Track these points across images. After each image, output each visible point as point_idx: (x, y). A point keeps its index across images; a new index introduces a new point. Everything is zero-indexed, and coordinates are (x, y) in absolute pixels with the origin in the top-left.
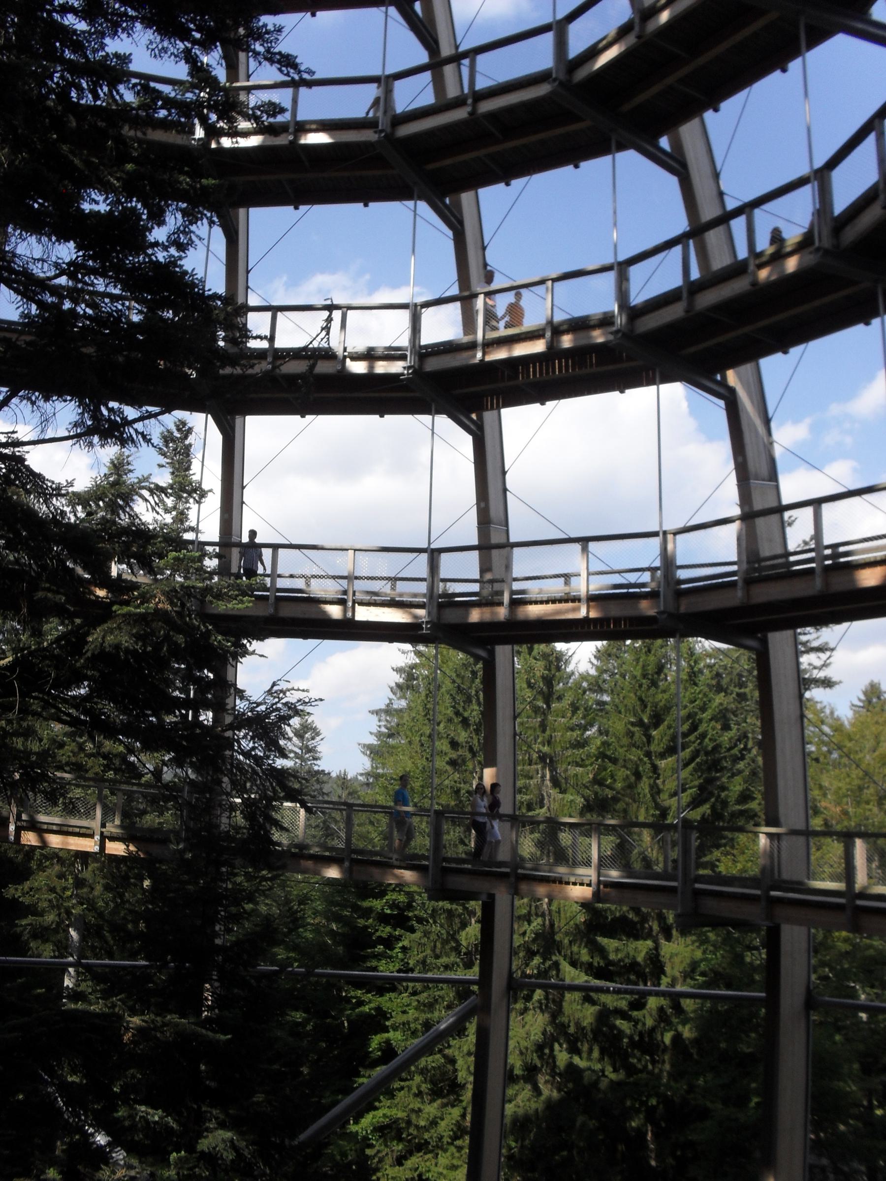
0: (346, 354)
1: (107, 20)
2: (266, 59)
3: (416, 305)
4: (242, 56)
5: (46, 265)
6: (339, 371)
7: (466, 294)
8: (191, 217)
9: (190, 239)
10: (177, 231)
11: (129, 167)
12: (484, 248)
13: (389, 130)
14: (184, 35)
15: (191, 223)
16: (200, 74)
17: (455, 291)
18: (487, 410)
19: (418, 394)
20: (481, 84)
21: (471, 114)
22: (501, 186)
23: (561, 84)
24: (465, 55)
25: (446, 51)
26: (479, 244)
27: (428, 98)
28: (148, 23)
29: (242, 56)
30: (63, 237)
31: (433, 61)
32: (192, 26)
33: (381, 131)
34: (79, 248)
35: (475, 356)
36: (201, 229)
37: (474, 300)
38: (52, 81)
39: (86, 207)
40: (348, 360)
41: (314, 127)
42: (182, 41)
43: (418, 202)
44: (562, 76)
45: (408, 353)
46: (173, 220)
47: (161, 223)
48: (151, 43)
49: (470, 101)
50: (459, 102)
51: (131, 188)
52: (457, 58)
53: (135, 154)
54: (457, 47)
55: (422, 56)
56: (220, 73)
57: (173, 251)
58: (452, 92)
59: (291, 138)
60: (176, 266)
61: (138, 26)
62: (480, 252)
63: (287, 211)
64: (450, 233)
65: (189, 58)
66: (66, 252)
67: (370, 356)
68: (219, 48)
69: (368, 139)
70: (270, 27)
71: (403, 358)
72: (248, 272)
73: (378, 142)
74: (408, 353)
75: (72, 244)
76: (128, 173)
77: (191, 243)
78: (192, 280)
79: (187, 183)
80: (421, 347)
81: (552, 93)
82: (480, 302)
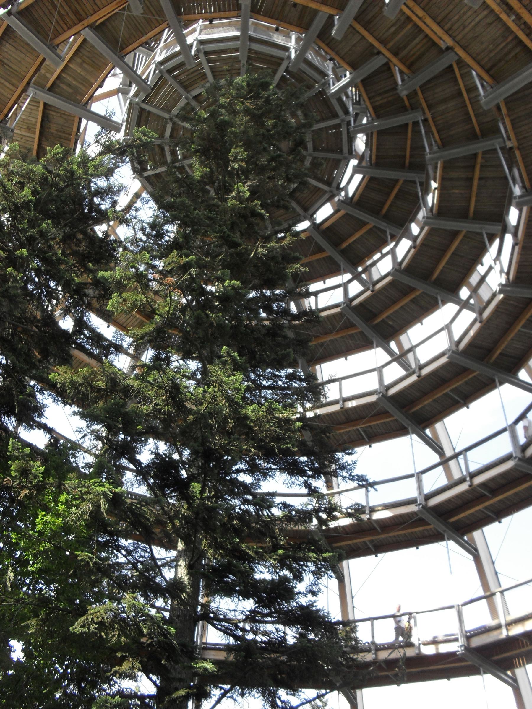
0: (420, 642)
1: (260, 473)
2: (350, 479)
3: (458, 606)
4: (334, 479)
5: (236, 613)
6: (417, 654)
7: (488, 594)
8: (318, 574)
9: (319, 588)
10: (312, 584)
11: (280, 552)
12: (493, 563)
13: (424, 503)
14: (302, 473)
15: (318, 578)
16: (313, 492)
17: (481, 593)
18: (517, 667)
19: (469, 663)
20: (473, 468)
21: (470, 486)
22: (496, 524)
23: (520, 459)
24: (460, 453)
25: (449, 453)
26: (490, 561)
27: (443, 481)
28: (282, 470)
29: (334, 479)
30: (246, 596)
31: (443, 460)
32: (307, 469)
33: (419, 505)
34: (256, 602)
35: (501, 633)
36: (324, 580)
37: (494, 597)
38: (235, 511)
39: (257, 576)
40: (422, 646)
41: (380, 508)
42: (302, 477)
43: (449, 542)
44: (519, 455)
45: (459, 637)
46: (308, 578)
47: (301, 580)
48: (285, 480)
49: (468, 479)
50: (462, 480)
51: (283, 563)
52: (456, 456)
53: (282, 543)
54: (454, 449)
55: (436, 458)
56: (324, 490)
57: (310, 596)
58: (457, 475)
59: (368, 516)
60: (313, 606)
61: (278, 473)
62: (492, 566)
63: (371, 558)
64: (471, 557)
65: (307, 485)
66: (249, 604)
67: (435, 642)
68: (323, 478)
69: (413, 510)
70: (350, 462)
71: (456, 640)
72: (352, 598)
73: (419, 511)
74: (459, 637)
75: (251, 601)
76: (280, 556)
77: (320, 590)
78: (323, 614)
79: (314, 558)
80: (466, 632)
81: (516, 465)
82: (498, 598)
